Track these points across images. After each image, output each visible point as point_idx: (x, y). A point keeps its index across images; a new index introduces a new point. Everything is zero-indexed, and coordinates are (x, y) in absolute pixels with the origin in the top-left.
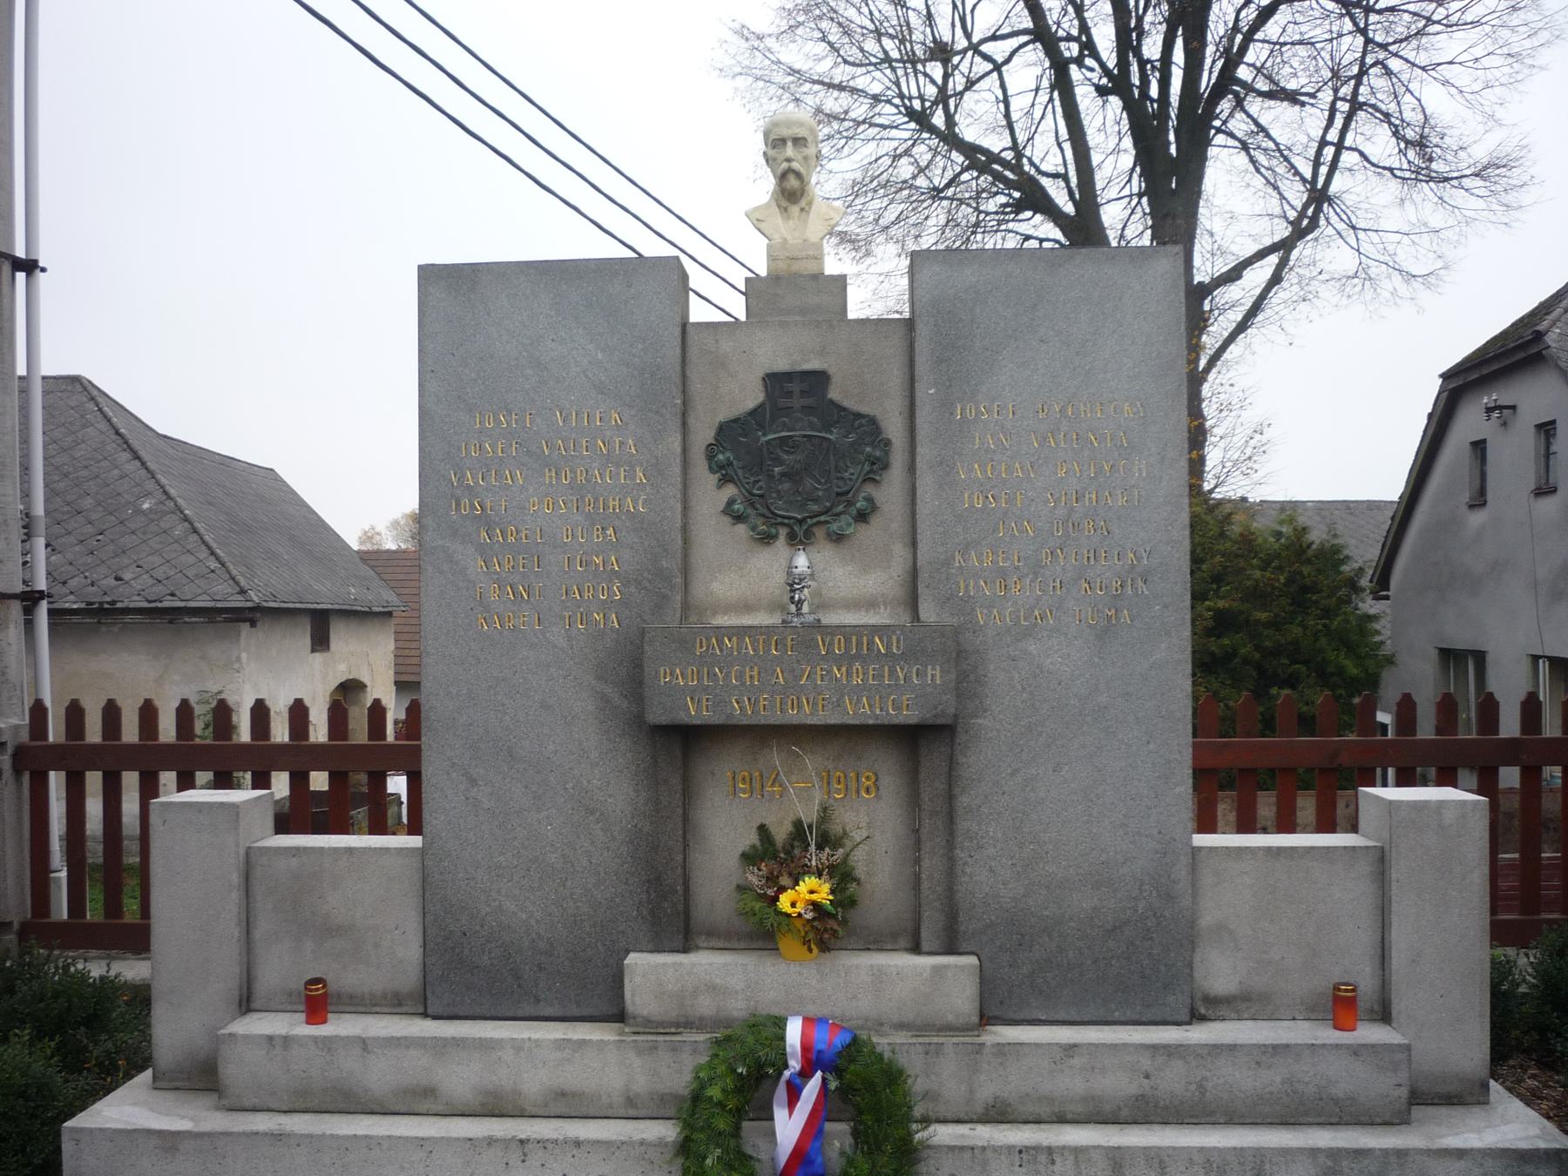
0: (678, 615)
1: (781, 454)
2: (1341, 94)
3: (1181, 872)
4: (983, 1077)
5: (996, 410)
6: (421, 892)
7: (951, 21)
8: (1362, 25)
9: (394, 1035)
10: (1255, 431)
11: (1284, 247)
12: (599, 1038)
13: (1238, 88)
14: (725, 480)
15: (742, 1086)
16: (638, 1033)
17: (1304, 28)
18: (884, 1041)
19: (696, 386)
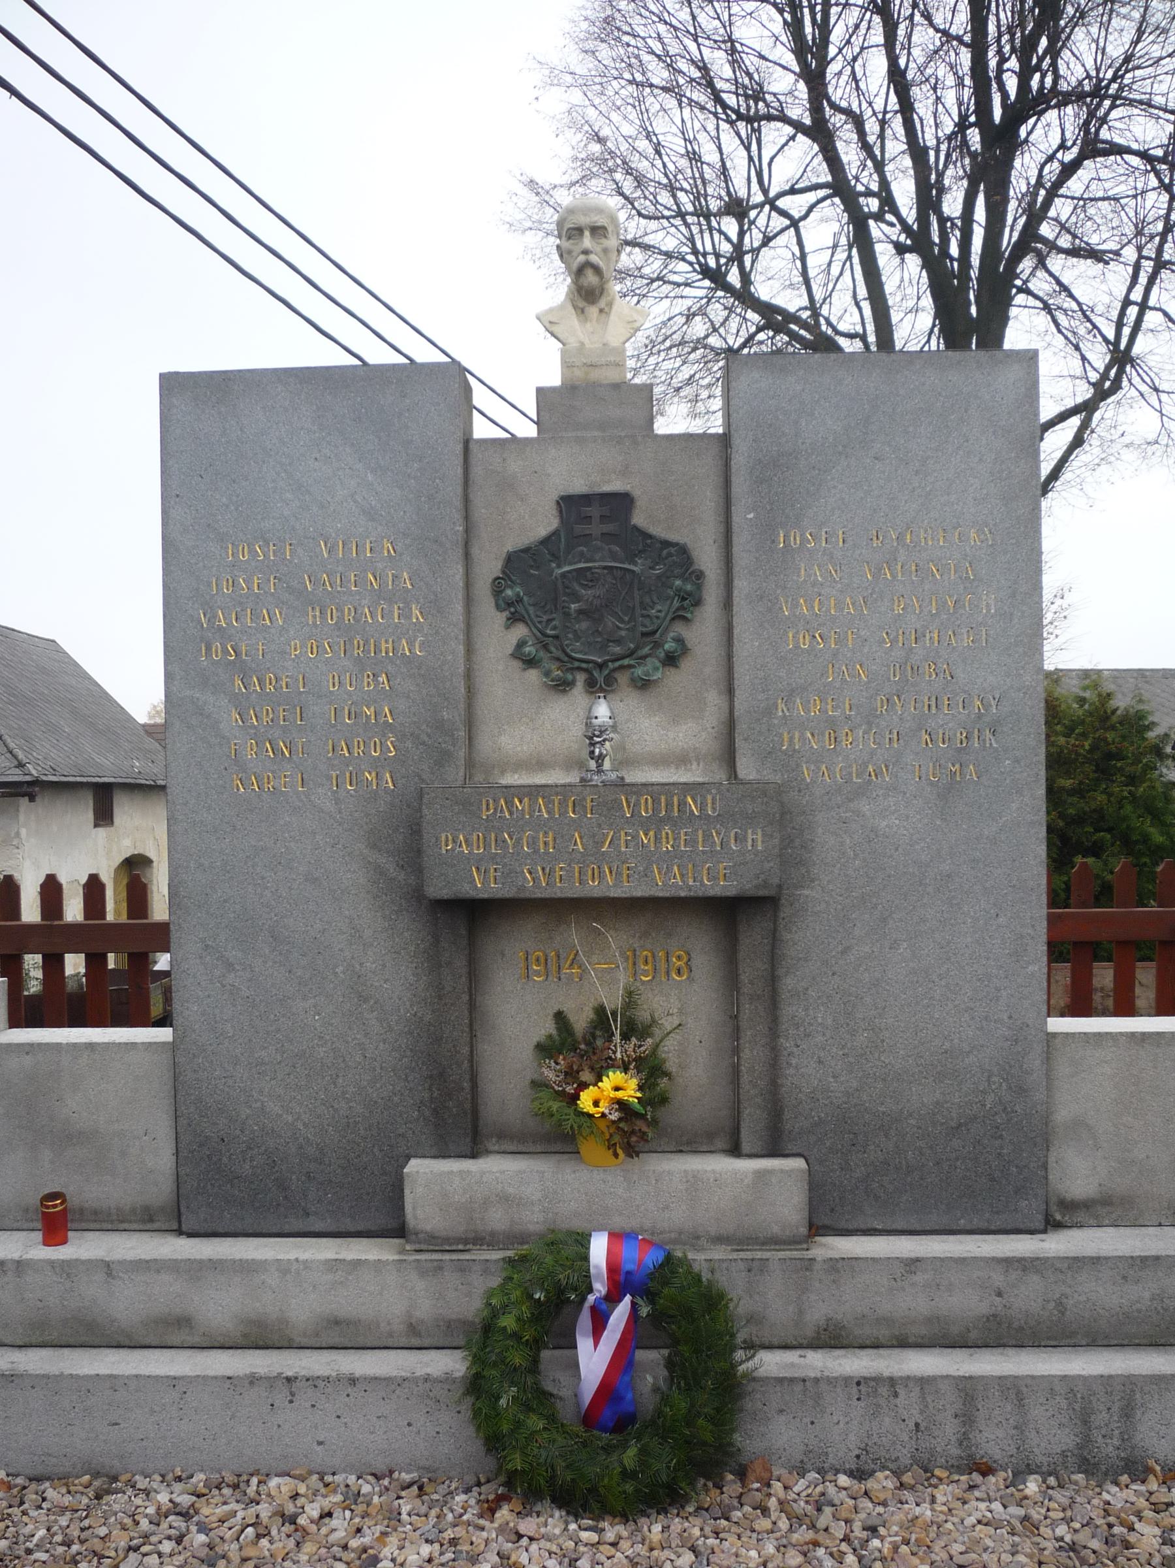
0: (461, 773)
1: (577, 588)
2: (1145, 253)
3: (1035, 1061)
4: (813, 1297)
5: (824, 538)
6: (173, 1092)
7: (746, 175)
8: (1167, 181)
9: (143, 1257)
10: (1056, 596)
11: (1087, 409)
12: (376, 1258)
13: (1040, 246)
14: (515, 619)
15: (541, 1313)
16: (421, 1251)
17: (1107, 185)
18: (701, 1257)
19: (480, 512)
